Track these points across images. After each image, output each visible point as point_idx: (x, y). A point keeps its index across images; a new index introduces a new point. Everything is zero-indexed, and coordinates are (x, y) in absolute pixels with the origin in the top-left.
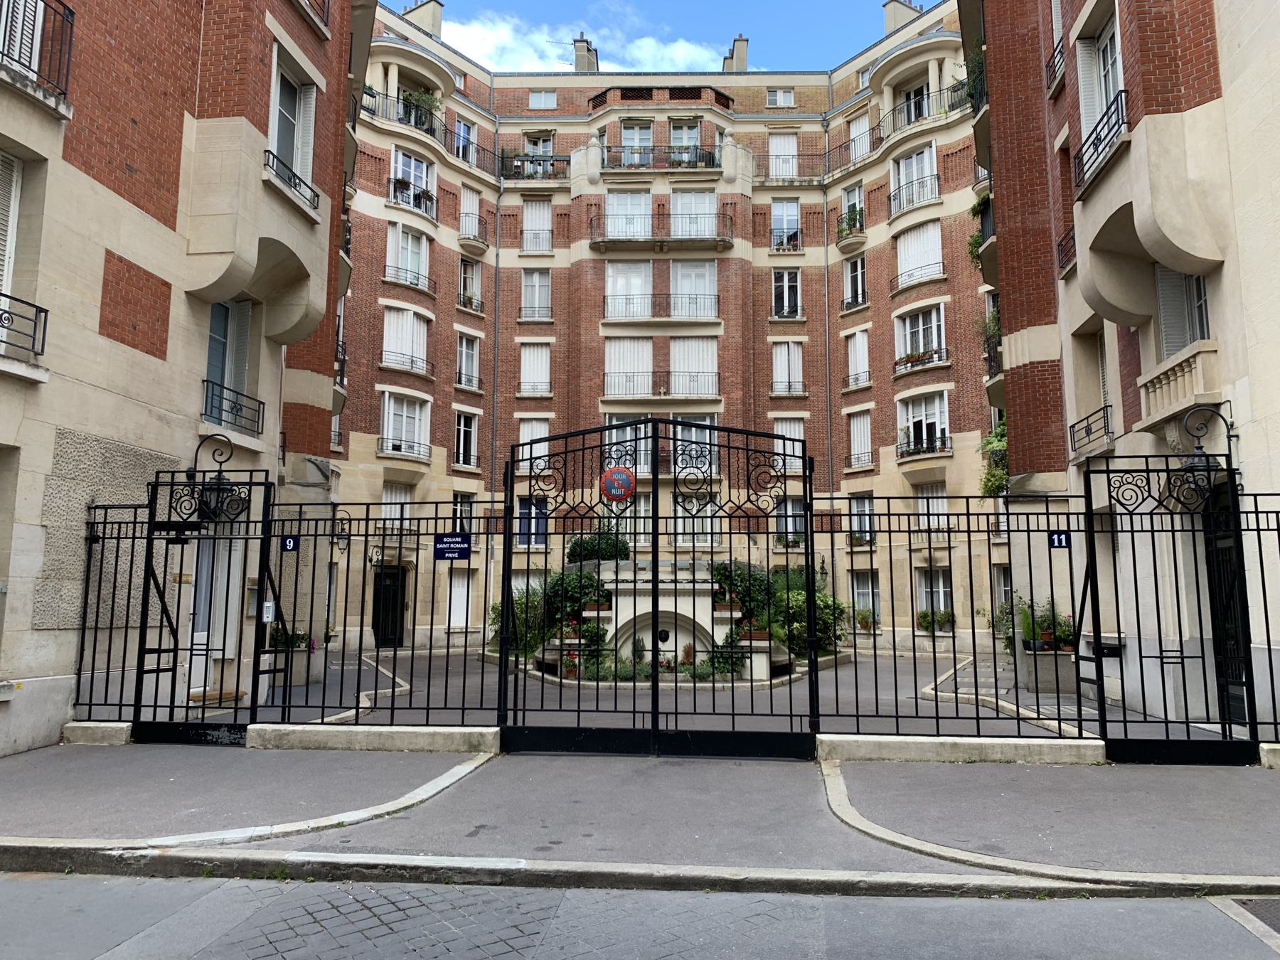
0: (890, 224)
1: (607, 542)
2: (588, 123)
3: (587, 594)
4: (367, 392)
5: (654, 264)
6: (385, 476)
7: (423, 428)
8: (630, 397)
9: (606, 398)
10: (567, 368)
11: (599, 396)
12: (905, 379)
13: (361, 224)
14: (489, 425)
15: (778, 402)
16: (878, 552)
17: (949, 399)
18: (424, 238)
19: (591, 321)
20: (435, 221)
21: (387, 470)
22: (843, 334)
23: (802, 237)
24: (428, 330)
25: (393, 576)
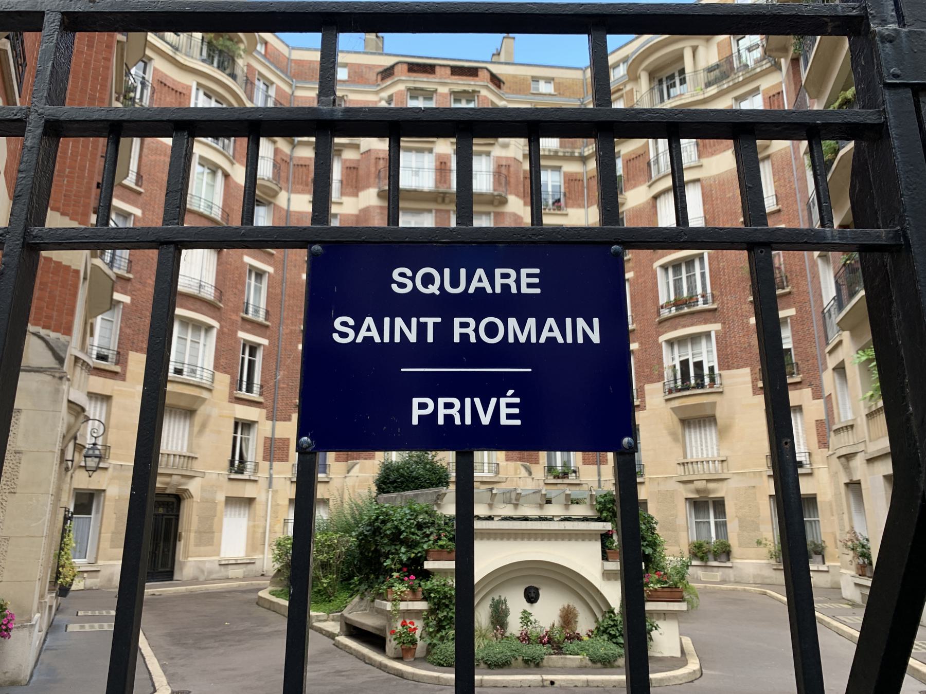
0: (650, 186)
1: (425, 468)
2: (377, 93)
5: (436, 213)
7: (207, 354)
12: (671, 321)
13: (157, 149)
16: (646, 483)
18: (220, 173)
20: (231, 158)
23: (566, 200)
24: (218, 259)
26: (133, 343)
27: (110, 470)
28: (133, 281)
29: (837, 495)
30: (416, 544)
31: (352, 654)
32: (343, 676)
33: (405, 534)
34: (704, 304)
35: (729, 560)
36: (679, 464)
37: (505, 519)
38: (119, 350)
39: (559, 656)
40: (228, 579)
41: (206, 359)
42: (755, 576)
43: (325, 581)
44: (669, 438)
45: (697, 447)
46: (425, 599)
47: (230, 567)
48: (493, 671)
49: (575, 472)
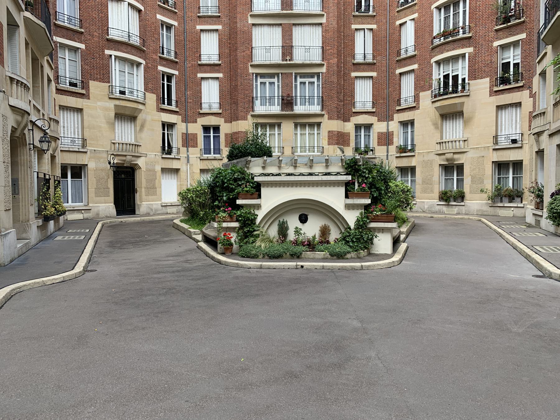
1: (256, 147)
3: (240, 185)
4: (100, 55)
6: (115, 110)
8: (268, 62)
9: (253, 63)
10: (229, 46)
11: (249, 62)
12: (439, 47)
14: (183, 81)
15: (358, 66)
16: (416, 156)
17: (469, 59)
19: (243, 13)
21: (116, 106)
22: (398, 23)
24: (139, 17)
25: (126, 173)
26: (91, 75)
27: (88, 153)
28: (84, 33)
29: (531, 159)
30: (233, 190)
31: (202, 251)
32: (187, 263)
33: (226, 184)
34: (463, 34)
35: (463, 201)
36: (437, 143)
37: (289, 175)
38: (83, 80)
39: (312, 252)
40: (167, 213)
41: (139, 84)
42: (477, 211)
43: (202, 213)
44: (432, 127)
45: (450, 132)
46: (237, 221)
47: (168, 207)
48: (272, 260)
49: (372, 150)
